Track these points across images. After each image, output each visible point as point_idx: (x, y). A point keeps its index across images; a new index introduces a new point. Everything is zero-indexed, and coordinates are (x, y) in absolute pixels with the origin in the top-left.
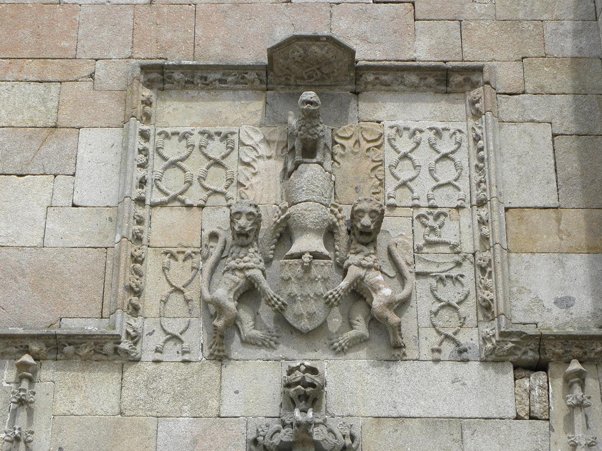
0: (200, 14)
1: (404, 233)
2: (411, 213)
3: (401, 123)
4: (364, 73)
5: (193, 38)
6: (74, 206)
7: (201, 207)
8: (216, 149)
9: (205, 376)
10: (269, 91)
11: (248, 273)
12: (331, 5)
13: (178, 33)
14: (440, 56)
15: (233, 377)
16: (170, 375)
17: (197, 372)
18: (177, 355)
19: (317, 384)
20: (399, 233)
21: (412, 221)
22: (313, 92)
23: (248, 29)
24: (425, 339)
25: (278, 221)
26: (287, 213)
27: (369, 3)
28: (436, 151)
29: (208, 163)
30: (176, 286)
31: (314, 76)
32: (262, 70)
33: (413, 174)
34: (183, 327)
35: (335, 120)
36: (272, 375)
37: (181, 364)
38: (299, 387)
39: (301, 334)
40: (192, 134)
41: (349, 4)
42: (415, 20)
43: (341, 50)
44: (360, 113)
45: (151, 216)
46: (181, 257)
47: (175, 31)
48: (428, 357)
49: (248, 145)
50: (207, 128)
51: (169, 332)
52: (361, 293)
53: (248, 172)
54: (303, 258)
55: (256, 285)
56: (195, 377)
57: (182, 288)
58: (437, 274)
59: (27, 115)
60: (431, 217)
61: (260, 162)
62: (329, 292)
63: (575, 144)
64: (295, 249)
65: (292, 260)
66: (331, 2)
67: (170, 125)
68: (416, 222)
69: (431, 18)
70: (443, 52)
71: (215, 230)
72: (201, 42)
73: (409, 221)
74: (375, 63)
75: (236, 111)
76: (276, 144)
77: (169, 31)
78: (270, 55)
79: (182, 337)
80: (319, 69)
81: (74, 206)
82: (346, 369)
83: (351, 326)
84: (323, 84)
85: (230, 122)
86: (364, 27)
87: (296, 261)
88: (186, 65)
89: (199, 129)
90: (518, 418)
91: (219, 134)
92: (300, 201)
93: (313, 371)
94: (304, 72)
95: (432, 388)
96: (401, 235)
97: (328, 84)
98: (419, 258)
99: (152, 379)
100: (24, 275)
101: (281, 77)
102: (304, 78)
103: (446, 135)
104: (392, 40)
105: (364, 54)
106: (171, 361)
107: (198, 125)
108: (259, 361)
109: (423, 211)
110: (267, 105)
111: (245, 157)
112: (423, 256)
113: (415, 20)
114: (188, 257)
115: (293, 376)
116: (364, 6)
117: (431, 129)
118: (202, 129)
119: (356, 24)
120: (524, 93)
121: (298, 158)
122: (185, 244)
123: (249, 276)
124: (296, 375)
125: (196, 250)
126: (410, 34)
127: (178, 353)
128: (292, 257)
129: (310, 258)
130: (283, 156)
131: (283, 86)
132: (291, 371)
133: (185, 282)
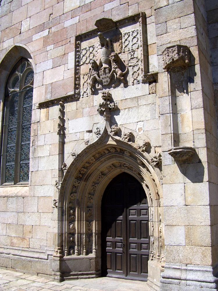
6: (68, 70)
9: (90, 99)
11: (94, 75)
46: (86, 75)
59: (60, 54)
60: (132, 52)
63: (149, 108)
74: (170, 87)
79: (86, 92)
81: (68, 70)
83: (99, 86)
89: (88, 46)
90: (150, 94)
99: (82, 101)
100: (61, 86)
103: (135, 32)
109: (130, 51)
120: (152, 16)
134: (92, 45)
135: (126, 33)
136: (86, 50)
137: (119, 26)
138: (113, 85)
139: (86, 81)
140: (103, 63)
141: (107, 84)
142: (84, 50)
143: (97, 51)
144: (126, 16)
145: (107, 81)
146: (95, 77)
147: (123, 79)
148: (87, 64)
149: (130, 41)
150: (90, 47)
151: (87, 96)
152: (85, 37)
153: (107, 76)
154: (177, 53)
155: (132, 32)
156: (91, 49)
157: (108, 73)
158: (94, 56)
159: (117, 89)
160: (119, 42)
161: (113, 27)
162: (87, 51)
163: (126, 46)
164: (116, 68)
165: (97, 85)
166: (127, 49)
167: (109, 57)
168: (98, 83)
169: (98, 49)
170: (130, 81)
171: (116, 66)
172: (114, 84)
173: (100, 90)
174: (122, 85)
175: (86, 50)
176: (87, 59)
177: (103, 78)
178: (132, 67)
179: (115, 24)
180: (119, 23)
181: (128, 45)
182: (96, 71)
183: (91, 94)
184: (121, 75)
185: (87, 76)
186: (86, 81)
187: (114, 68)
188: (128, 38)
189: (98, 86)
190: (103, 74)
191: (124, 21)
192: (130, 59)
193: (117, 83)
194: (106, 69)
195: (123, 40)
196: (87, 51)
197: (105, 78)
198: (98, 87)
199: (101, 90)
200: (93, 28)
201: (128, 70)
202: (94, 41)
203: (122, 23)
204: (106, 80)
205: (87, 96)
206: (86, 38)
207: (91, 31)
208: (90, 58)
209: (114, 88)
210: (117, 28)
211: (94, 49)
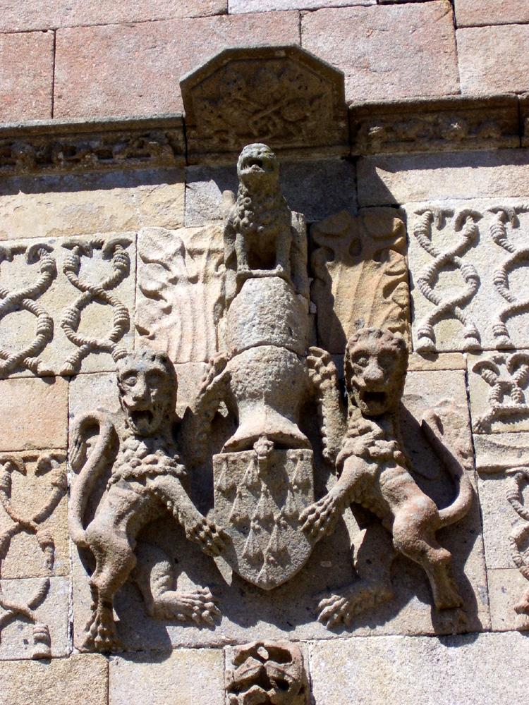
0: (62, 43)
1: (451, 399)
2: (464, 363)
3: (438, 204)
4: (363, 122)
5: (51, 85)
7: (70, 376)
8: (96, 271)
9: (78, 683)
10: (191, 166)
11: (152, 484)
12: (301, 13)
13: (24, 80)
14: (505, 85)
15: (132, 683)
16: (10, 684)
17: (63, 677)
18: (24, 646)
19: (290, 681)
20: (442, 400)
21: (466, 375)
22: (263, 145)
23: (150, 63)
24: (500, 591)
25: (210, 386)
26: (224, 371)
27: (370, 5)
28: (506, 248)
29: (80, 296)
30: (22, 519)
31: (271, 128)
32: (176, 128)
33: (465, 290)
34: (36, 593)
35: (314, 208)
36: (207, 674)
37: (33, 662)
38: (255, 687)
39: (262, 595)
40: (50, 250)
41: (333, 9)
42: (456, 28)
43: (315, 74)
44: (361, 191)
45: (72, 624)
46: (32, 467)
47: (19, 75)
48: (507, 624)
49: (153, 262)
50: (77, 237)
51: (8, 604)
52: (372, 510)
53: (155, 307)
54: (255, 447)
55: (169, 503)
56: (60, 686)
57: (33, 524)
58: (518, 469)
60: (503, 368)
61: (181, 290)
62: (310, 508)
64: (240, 434)
65: (236, 453)
66: (300, 8)
67: (10, 236)
68: (472, 375)
69: (485, 22)
70: (511, 79)
71: (93, 412)
72: (64, 90)
73: (459, 376)
75: (130, 204)
76: (205, 255)
77: (8, 77)
78: (253, 245)
79: (35, 614)
80: (277, 113)
82: (349, 655)
84: (286, 145)
85: (119, 223)
86: (362, 46)
87: (243, 454)
88: (36, 126)
91: (98, 245)
92: (247, 345)
93: (280, 655)
94: (251, 123)
95: (520, 683)
96: (446, 402)
97: (300, 144)
98: (483, 443)
101: (210, 138)
102: (252, 134)
104: (416, 64)
105: (497, 351)
106: (13, 657)
107: (62, 232)
108: (182, 649)
109: (486, 357)
110: (187, 189)
111: (149, 282)
112: (491, 438)
113: (456, 28)
114: (44, 468)
115: (243, 667)
116: (361, 11)
117: (494, 211)
118: (67, 240)
119: (348, 42)
121: (243, 268)
122: (39, 444)
123: (156, 489)
124: (248, 666)
125: (59, 452)
126: (449, 50)
127: (26, 642)
128: (236, 447)
129: (268, 446)
130: (218, 276)
131: (217, 154)
132: (239, 661)
133: (39, 511)
134: (108, 238)
135: (448, 214)
136: (38, 266)
137: (376, 144)
138: (331, 603)
139: (40, 519)
140: (254, 396)
141: (279, 579)
142: (21, 259)
143: (154, 295)
144: (440, 90)
145: (281, 557)
146: (158, 500)
147: (444, 560)
148: (49, 377)
149: (487, 283)
150: (84, 251)
151: (45, 658)
152: (44, 161)
153: (287, 509)
154: (55, 485)
155: (505, 218)
156: (96, 271)
157: (304, 487)
158: (124, 326)
159: (361, 641)
160: (386, 266)
161: (320, 147)
162: (52, 272)
163: (448, 313)
164: (384, 461)
165: (159, 571)
166: (452, 336)
167: (311, 364)
168: (170, 562)
169: (174, 281)
170: (496, 595)
171: (384, 446)
172: (339, 589)
173: (187, 622)
174: (417, 613)
175: (44, 261)
176: (48, 335)
177: (242, 526)
178: (511, 483)
179: (342, 124)
180: (382, 122)
181: (464, 302)
182: (167, 453)
183: (90, 646)
184: (434, 530)
185: (50, 477)
186: (40, 519)
187: (366, 456)
188: (462, 251)
189: (172, 585)
190: (254, 489)
191: (430, 118)
192: (493, 419)
193: (374, 588)
194: (292, 453)
195: (420, 262)
196: (52, 272)
197: (267, 522)
198: (169, 596)
199: (201, 624)
200: (111, 106)
201: (474, 497)
202: (129, 215)
203: (411, 134)
204: (271, 541)
205: (38, 658)
206: (47, 174)
207: (75, 129)
208: (82, 334)
209: (341, 624)
210: (352, 161)
211: (125, 272)
